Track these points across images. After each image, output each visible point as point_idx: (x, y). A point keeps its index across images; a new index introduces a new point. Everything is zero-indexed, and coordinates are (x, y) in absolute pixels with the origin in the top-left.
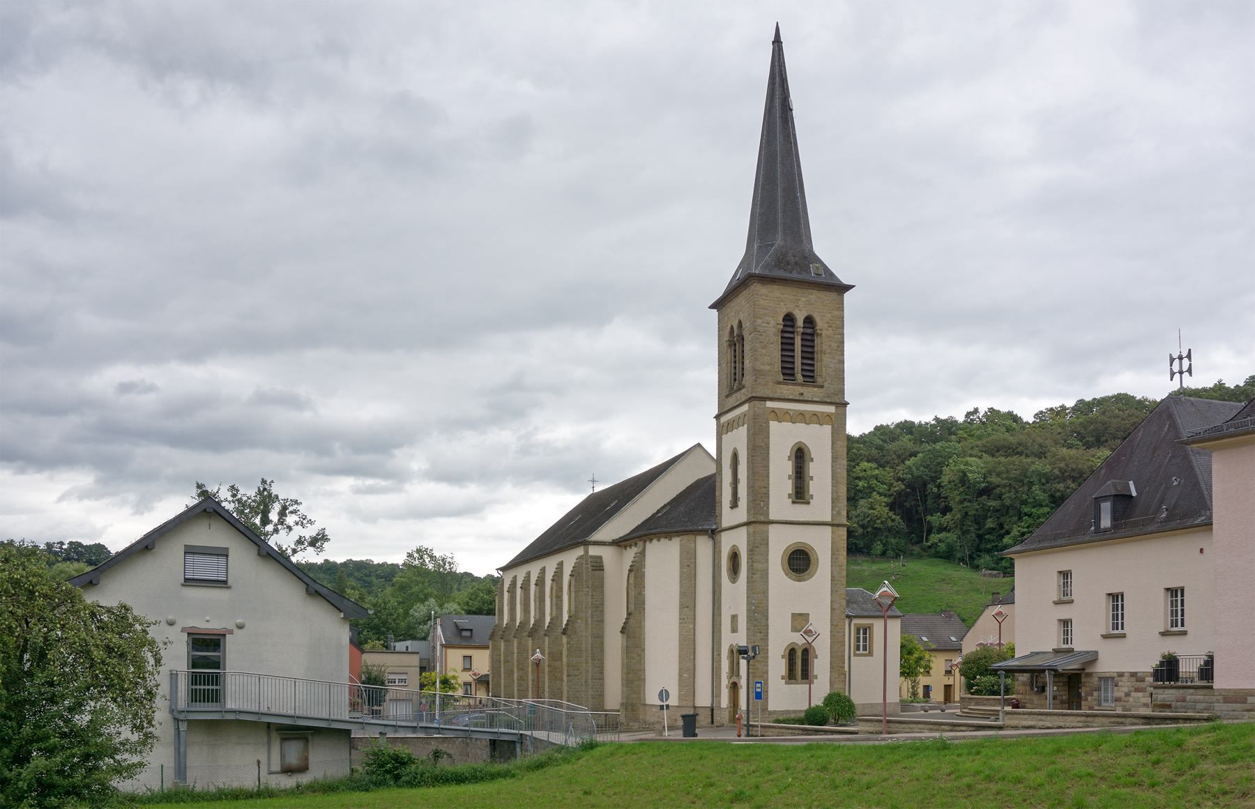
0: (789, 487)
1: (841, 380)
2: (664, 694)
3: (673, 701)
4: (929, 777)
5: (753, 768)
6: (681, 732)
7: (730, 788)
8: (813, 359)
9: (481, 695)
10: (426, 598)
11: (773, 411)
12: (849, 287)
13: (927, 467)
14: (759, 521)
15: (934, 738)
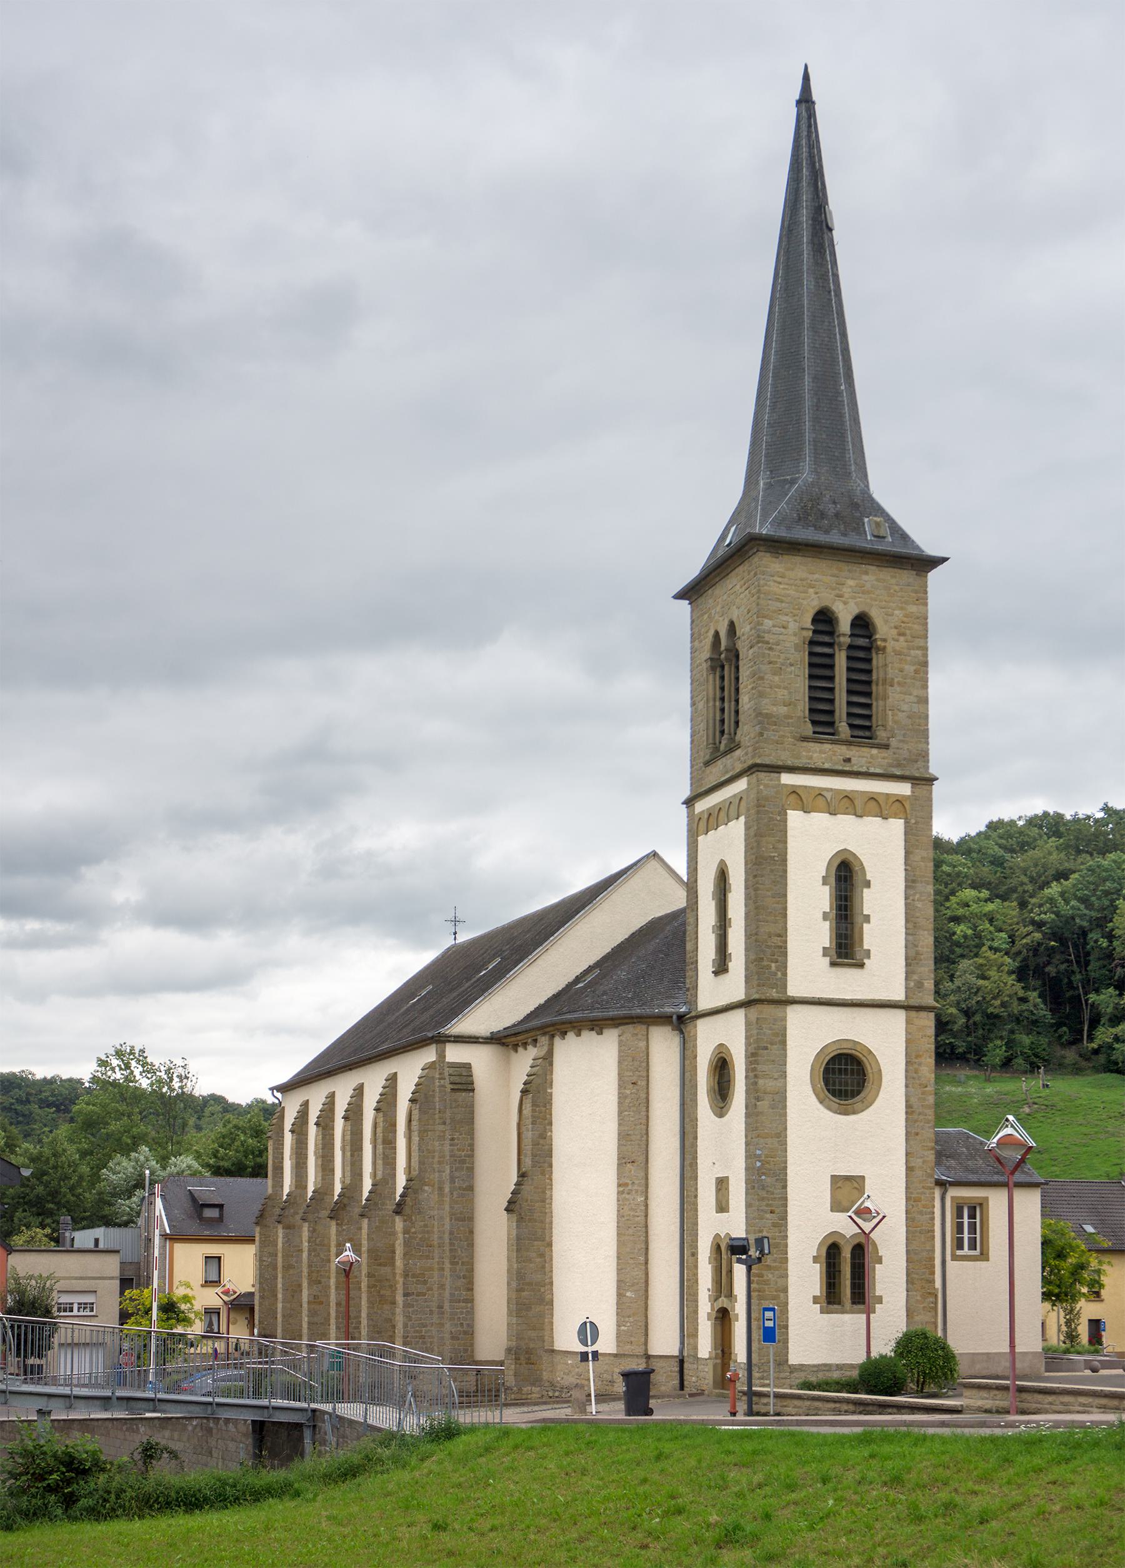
0: (823, 934)
1: (923, 734)
2: (588, 1332)
3: (606, 1344)
4: (1102, 1504)
5: (758, 1478)
6: (621, 1406)
7: (714, 1518)
8: (869, 694)
9: (239, 1332)
10: (134, 1147)
11: (794, 791)
12: (934, 562)
13: (1084, 900)
14: (767, 998)
15: (1110, 1424)
